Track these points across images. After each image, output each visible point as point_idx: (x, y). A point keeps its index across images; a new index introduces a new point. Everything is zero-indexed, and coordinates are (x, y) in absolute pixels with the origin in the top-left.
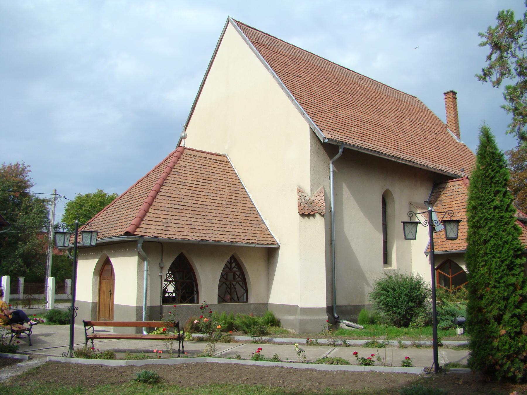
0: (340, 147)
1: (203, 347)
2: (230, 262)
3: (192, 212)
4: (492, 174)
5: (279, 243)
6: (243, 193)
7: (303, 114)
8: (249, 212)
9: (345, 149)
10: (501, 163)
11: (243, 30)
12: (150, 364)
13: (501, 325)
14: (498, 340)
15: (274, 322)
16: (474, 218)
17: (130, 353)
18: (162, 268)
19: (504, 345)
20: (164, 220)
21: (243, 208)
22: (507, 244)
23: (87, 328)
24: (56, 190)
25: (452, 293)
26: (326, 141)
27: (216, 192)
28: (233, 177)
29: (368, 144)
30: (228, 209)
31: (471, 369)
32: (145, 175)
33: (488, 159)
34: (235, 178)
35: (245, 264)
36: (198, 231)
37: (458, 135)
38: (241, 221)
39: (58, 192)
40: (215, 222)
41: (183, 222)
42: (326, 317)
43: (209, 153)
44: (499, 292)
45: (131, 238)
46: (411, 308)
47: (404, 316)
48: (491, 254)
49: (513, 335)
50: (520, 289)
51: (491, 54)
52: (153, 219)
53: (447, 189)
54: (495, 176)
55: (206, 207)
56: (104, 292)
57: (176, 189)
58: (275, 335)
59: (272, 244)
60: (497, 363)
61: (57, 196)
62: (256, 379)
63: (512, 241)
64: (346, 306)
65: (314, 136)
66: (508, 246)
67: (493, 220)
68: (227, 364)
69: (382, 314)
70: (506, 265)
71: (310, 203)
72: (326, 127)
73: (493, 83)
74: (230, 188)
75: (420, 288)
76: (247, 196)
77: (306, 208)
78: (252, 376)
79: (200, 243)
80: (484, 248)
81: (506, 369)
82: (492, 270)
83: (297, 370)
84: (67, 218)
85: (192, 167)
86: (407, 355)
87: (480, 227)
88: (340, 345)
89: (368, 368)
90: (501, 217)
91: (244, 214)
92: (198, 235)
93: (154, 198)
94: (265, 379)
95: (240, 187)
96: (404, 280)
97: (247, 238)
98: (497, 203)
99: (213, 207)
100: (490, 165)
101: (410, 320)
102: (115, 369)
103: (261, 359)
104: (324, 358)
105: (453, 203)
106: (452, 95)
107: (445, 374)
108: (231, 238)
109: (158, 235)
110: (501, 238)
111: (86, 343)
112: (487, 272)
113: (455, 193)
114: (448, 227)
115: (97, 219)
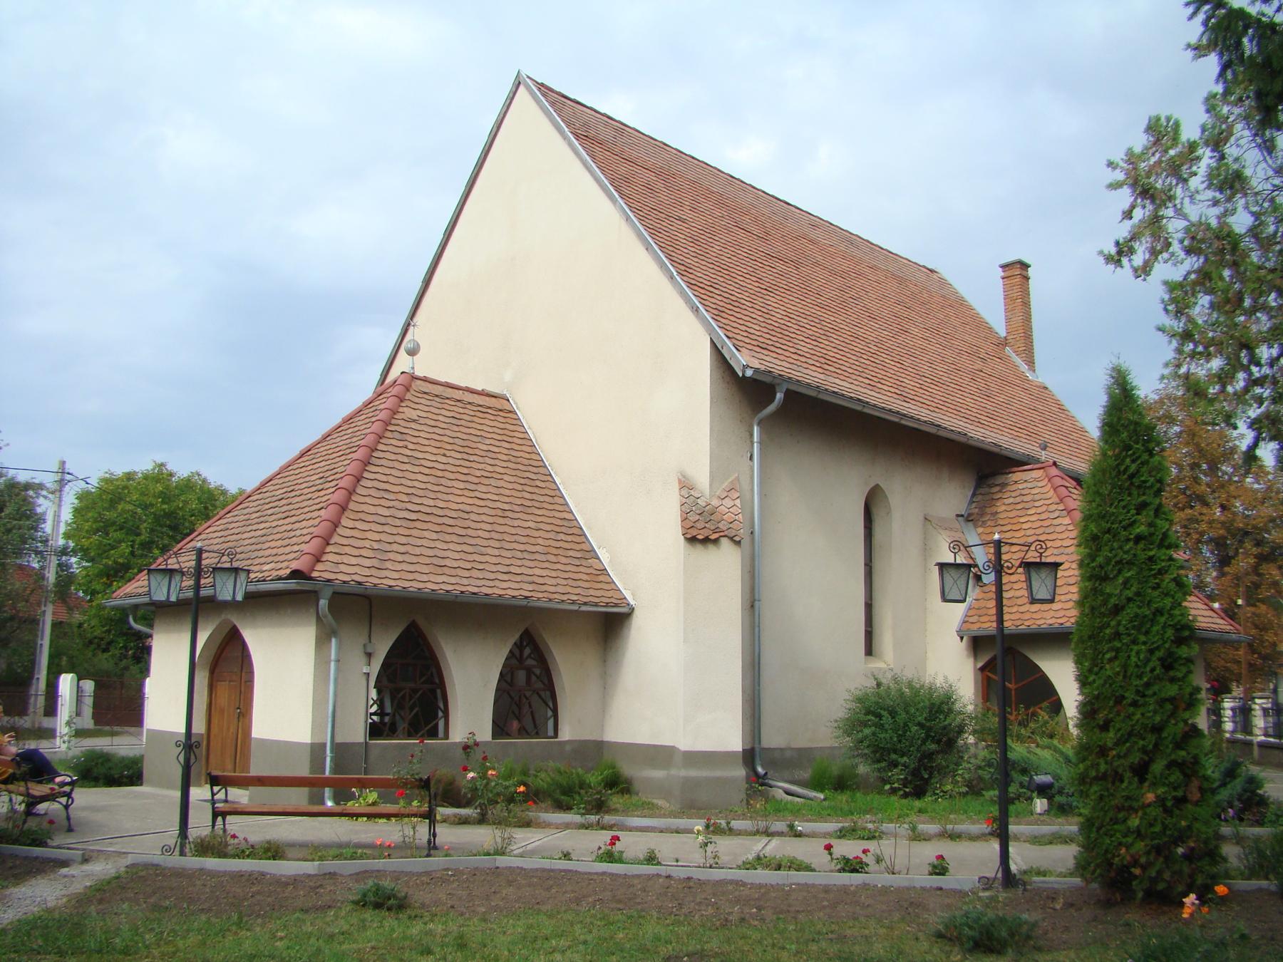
0: (777, 388)
1: (484, 836)
2: (519, 646)
3: (437, 528)
4: (1133, 467)
5: (632, 602)
6: (547, 484)
7: (696, 310)
8: (563, 529)
9: (789, 394)
10: (1152, 445)
11: (553, 104)
12: (373, 871)
13: (1146, 784)
14: (1140, 814)
15: (617, 784)
16: (1093, 560)
17: (315, 850)
18: (369, 655)
19: (1151, 825)
20: (376, 546)
21: (549, 520)
22: (1162, 614)
23: (216, 789)
24: (64, 463)
25: (1020, 724)
26: (749, 373)
27: (486, 481)
28: (524, 448)
29: (837, 381)
30: (516, 523)
31: (1082, 876)
32: (318, 437)
33: (1125, 435)
34: (529, 449)
35: (555, 652)
36: (453, 572)
37: (1031, 363)
38: (546, 550)
39: (69, 467)
40: (489, 551)
41: (417, 551)
42: (740, 772)
43: (468, 390)
44: (1143, 714)
45: (306, 585)
46: (930, 756)
47: (915, 773)
48: (1129, 635)
49: (1169, 804)
50: (1185, 710)
51: (1133, 207)
52: (351, 541)
53: (1009, 488)
54: (1138, 471)
55: (466, 516)
56: (222, 711)
57: (400, 474)
58: (626, 812)
59: (616, 605)
60: (1135, 863)
61: (68, 477)
62: (619, 901)
63: (1171, 609)
64: (781, 749)
65: (721, 361)
66: (1162, 620)
67: (1133, 564)
68: (544, 870)
69: (863, 769)
70: (1159, 659)
71: (709, 514)
72: (747, 340)
73: (1135, 270)
74: (518, 473)
75: (950, 710)
76: (556, 494)
77: (699, 525)
78: (608, 895)
79: (459, 600)
80: (1113, 623)
81: (1154, 874)
82: (1131, 670)
83: (701, 883)
84: (78, 529)
85: (433, 423)
86: (935, 854)
87: (1105, 579)
88: (780, 834)
89: (857, 878)
90: (1151, 559)
91: (552, 535)
92: (453, 580)
93: (351, 492)
94: (638, 900)
95: (541, 470)
96: (916, 692)
97: (560, 589)
98: (1141, 529)
99: (484, 518)
100: (1130, 448)
101: (927, 781)
102: (295, 881)
103: (620, 861)
104: (758, 858)
105: (1022, 520)
106: (1017, 272)
107: (1025, 890)
108: (525, 590)
109: (365, 579)
110: (1150, 602)
111: (213, 826)
112: (1118, 674)
113: (1025, 499)
114: (1034, 576)
115: (202, 537)
